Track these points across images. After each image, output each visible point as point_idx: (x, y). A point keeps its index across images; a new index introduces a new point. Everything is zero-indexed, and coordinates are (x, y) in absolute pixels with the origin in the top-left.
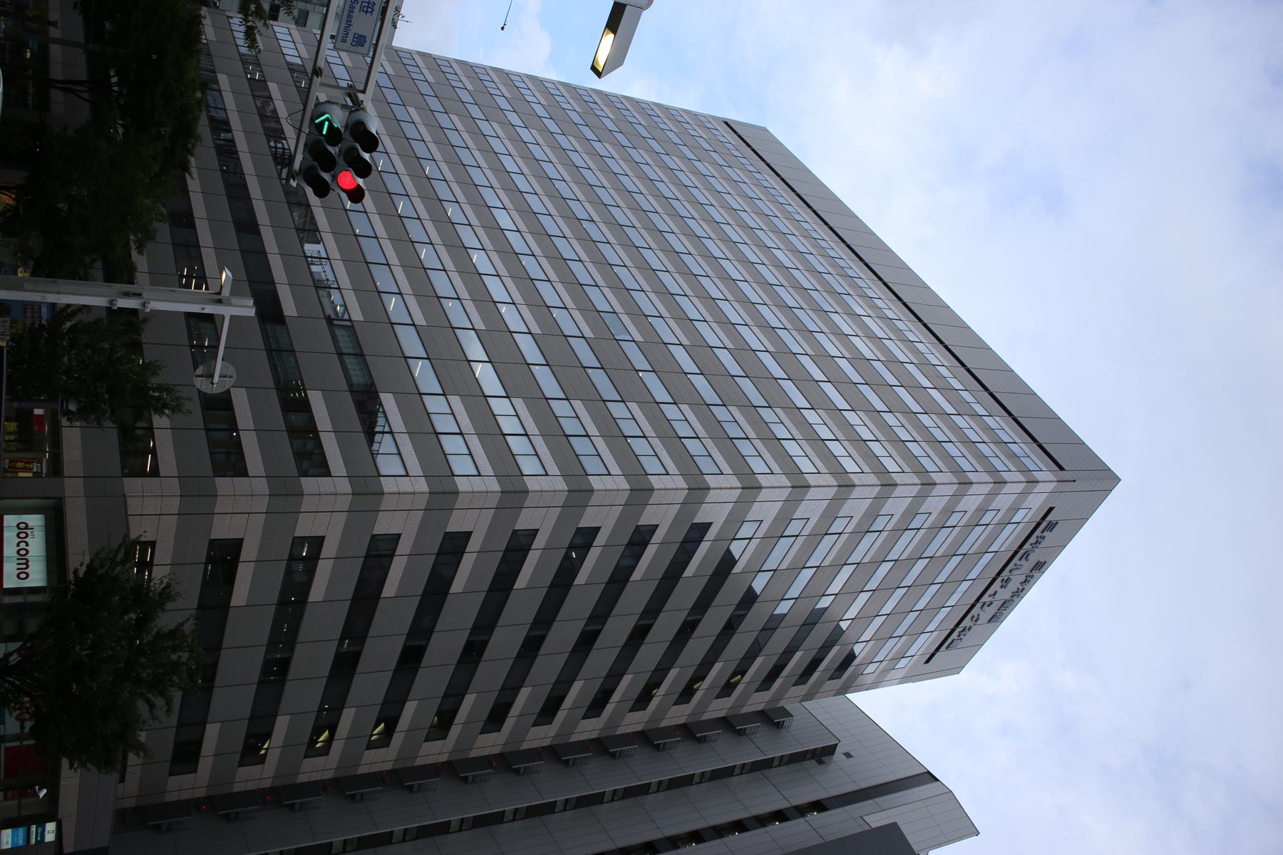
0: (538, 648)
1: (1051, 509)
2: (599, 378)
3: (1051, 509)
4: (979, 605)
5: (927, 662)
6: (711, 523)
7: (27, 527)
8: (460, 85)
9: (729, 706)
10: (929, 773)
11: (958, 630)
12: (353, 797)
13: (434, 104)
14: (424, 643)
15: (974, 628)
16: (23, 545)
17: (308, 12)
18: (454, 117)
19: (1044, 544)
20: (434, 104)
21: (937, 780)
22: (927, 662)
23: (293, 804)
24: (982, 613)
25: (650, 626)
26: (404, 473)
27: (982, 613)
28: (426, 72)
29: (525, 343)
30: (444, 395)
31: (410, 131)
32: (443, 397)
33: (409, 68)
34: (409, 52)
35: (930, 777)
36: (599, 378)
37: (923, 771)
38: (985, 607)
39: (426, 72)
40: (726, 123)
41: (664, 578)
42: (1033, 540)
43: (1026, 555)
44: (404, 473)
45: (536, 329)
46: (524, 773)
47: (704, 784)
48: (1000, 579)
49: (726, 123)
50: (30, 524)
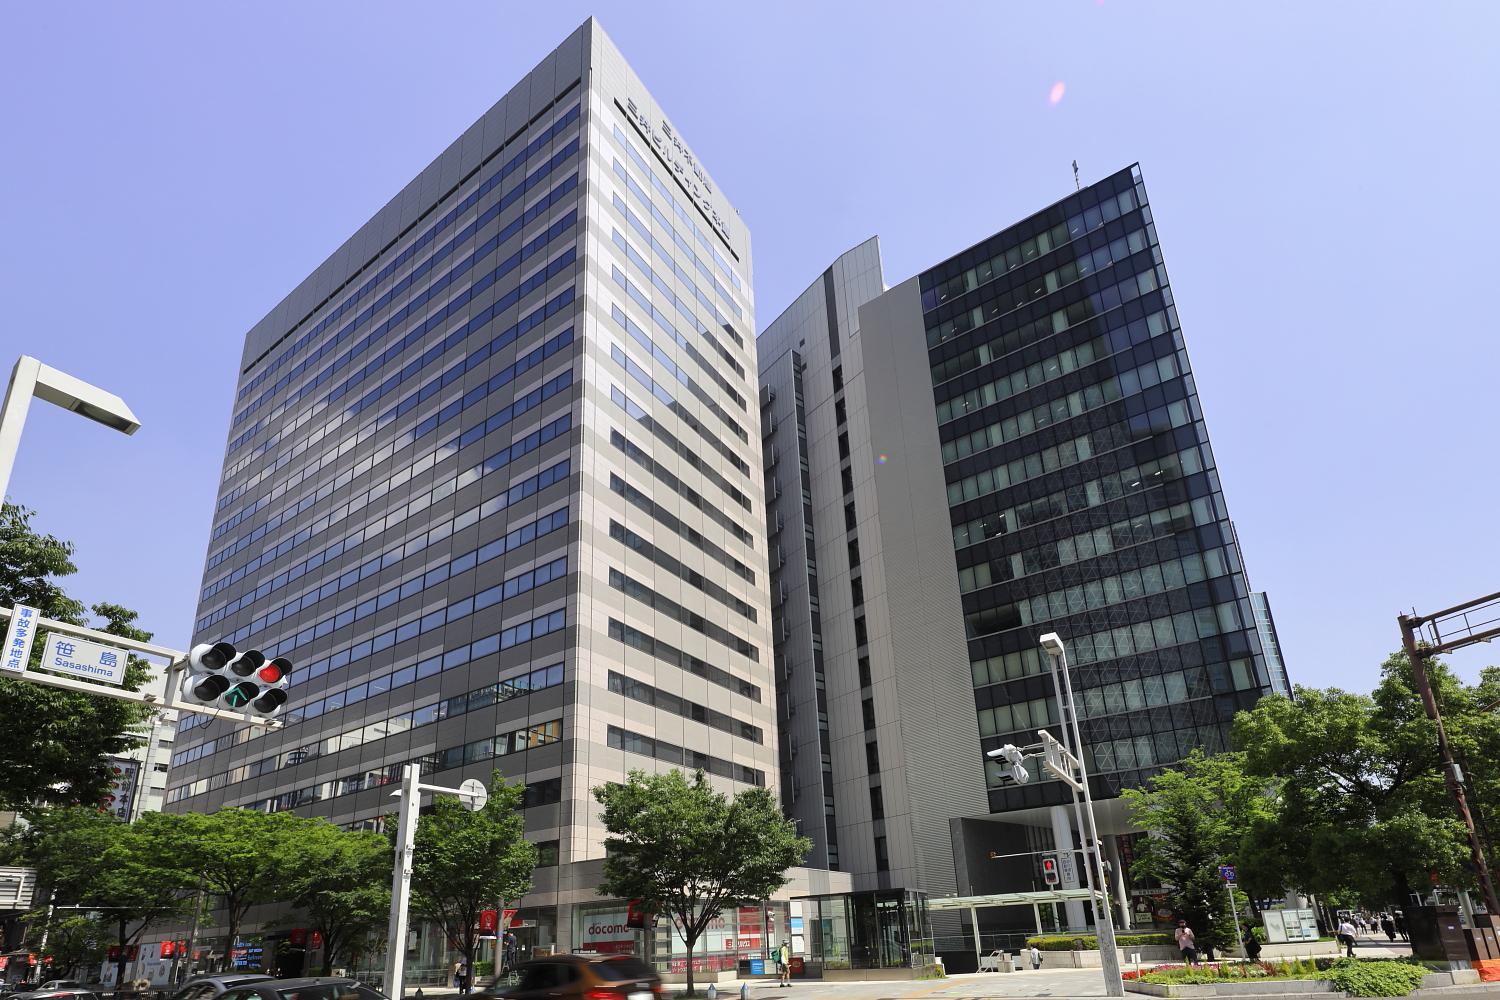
0: (704, 756)
1: (616, 102)
2: (482, 601)
3: (616, 102)
4: (695, 199)
5: (737, 259)
6: (611, 520)
7: (593, 928)
8: (222, 612)
9: (748, 313)
10: (825, 274)
11: (714, 223)
12: (786, 637)
13: (248, 600)
14: (689, 615)
15: (714, 209)
16: (605, 930)
17: (161, 741)
18: (255, 618)
19: (646, 119)
20: (248, 600)
21: (831, 267)
22: (737, 259)
23: (793, 754)
24: (703, 198)
25: (690, 529)
26: (562, 665)
27: (703, 198)
28: (216, 608)
29: (453, 660)
30: (501, 633)
31: (274, 618)
32: (503, 634)
33: (214, 621)
34: (204, 591)
35: (828, 274)
36: (482, 601)
37: (822, 278)
38: (698, 193)
39: (216, 608)
40: (245, 372)
41: (653, 605)
42: (642, 129)
43: (657, 140)
44: (562, 665)
45: (454, 472)
46: (782, 525)
47: (815, 529)
48: (674, 172)
49: (245, 372)
50: (590, 925)
